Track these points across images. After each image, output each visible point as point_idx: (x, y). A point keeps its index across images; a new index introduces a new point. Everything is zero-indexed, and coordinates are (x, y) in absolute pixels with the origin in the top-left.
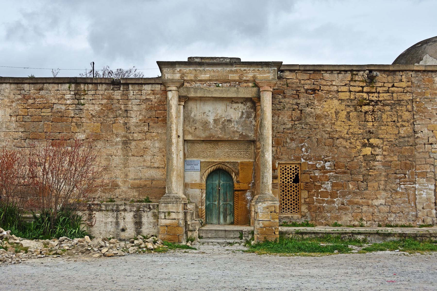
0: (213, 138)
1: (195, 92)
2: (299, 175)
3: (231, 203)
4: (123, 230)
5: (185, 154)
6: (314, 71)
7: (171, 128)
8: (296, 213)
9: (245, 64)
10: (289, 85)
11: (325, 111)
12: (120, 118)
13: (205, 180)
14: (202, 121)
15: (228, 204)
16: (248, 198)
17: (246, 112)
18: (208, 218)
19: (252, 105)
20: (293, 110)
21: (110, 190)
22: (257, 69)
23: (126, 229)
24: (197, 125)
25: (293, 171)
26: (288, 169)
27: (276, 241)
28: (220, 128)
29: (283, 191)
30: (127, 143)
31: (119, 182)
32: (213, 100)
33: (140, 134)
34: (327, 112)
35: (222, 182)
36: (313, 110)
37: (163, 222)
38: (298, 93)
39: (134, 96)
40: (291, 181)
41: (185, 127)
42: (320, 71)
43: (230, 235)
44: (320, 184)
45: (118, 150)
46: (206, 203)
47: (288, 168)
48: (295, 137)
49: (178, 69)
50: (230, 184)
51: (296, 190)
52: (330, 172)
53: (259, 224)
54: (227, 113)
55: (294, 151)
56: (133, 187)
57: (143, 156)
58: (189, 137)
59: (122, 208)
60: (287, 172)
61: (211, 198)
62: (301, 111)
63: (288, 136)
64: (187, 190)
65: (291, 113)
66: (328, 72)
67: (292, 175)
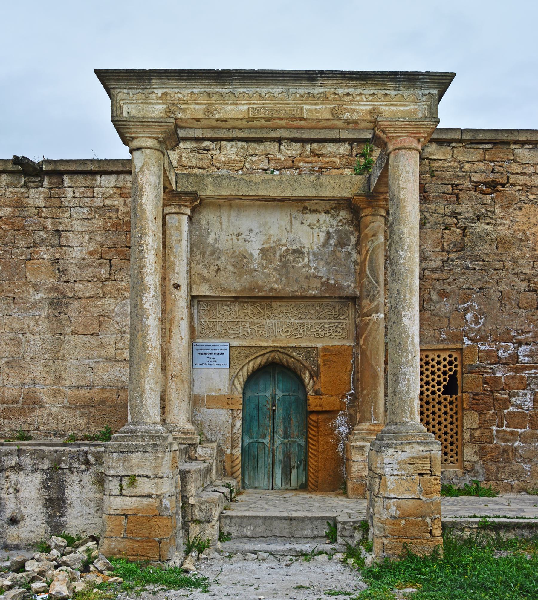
0: (259, 291)
1: (217, 185)
2: (458, 376)
3: (302, 441)
4: (14, 521)
5: (192, 329)
6: (495, 143)
7: (140, 245)
8: (452, 462)
9: (349, 79)
10: (436, 173)
11: (519, 230)
12: (43, 248)
13: (239, 389)
14: (234, 252)
15: (294, 442)
16: (341, 429)
17: (337, 232)
18: (247, 473)
19: (350, 217)
20: (446, 229)
21: (21, 412)
22: (384, 92)
23: (23, 518)
24: (222, 262)
25: (445, 366)
26: (432, 363)
27: (435, 552)
28: (276, 269)
29: (427, 383)
30: (61, 304)
31: (42, 395)
32: (259, 206)
33: (90, 285)
34: (524, 232)
35: (279, 394)
36: (490, 228)
37: (117, 504)
38: (456, 191)
39: (77, 200)
40: (439, 390)
41: (194, 264)
42: (508, 143)
43: (302, 529)
44: (506, 396)
45: (38, 322)
46: (243, 441)
47: (433, 360)
48: (449, 288)
49: (159, 92)
50: (297, 399)
51: (451, 410)
52: (530, 368)
53: (386, 508)
54: (291, 236)
55: (447, 320)
56: (74, 405)
57: (97, 334)
58: (203, 290)
59: (13, 461)
60: (431, 369)
61: (255, 430)
62: (464, 229)
63: (433, 285)
65: (440, 236)
66: (527, 146)
67: (443, 377)
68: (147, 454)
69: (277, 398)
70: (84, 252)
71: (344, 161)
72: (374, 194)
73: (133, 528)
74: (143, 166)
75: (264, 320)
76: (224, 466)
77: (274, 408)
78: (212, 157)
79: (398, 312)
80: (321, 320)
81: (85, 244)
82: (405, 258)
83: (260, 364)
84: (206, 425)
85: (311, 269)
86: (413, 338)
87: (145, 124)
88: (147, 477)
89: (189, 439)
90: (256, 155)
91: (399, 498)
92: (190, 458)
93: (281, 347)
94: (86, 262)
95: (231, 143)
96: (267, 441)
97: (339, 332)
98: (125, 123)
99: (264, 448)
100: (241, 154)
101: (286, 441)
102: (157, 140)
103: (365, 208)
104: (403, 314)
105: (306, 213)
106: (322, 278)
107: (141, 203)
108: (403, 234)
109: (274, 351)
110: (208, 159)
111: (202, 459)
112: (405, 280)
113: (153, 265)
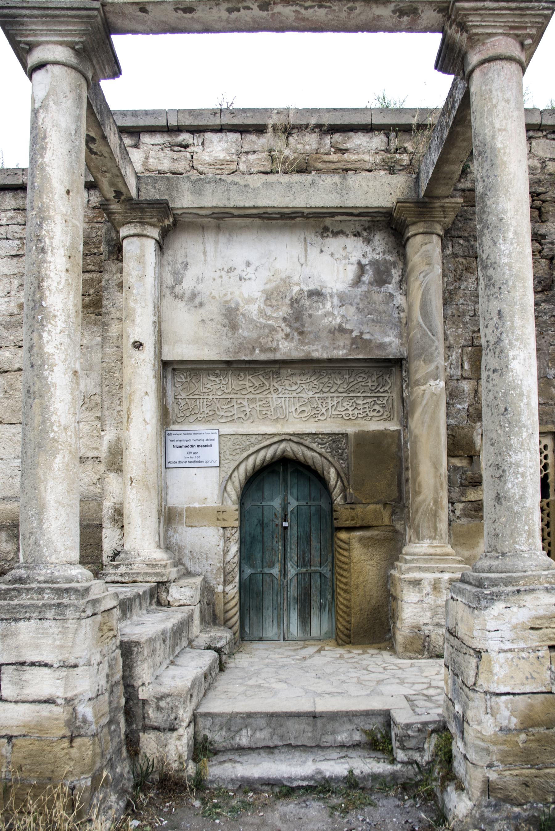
1: (197, 191)
3: (326, 570)
7: (39, 239)
13: (234, 497)
15: (315, 572)
18: (247, 621)
32: (260, 228)
35: (293, 504)
43: (333, 733)
46: (241, 572)
50: (319, 510)
53: (492, 712)
61: (259, 556)
64: (176, 531)
68: (47, 624)
69: (290, 508)
70: (12, 304)
71: (378, 159)
72: (427, 200)
73: (23, 762)
74: (47, 97)
75: (269, 396)
76: (214, 611)
77: (286, 524)
78: (192, 157)
79: (502, 351)
80: (351, 395)
81: (13, 293)
82: (510, 253)
83: (264, 460)
84: (187, 552)
85: (335, 319)
86: (529, 397)
87: (49, 12)
88: (46, 665)
89: (157, 574)
90: (254, 152)
91: (514, 694)
92: (159, 603)
93: (294, 435)
94: (14, 319)
95: (219, 135)
96: (276, 571)
97: (379, 411)
98: (14, 11)
99: (272, 581)
100: (233, 151)
101: (304, 570)
102: (73, 49)
103: (414, 223)
104: (511, 354)
105: (328, 236)
106: (351, 331)
107: (42, 164)
108: (505, 212)
109: (284, 440)
110: (186, 159)
111: (177, 604)
112: (512, 294)
113: (63, 274)
